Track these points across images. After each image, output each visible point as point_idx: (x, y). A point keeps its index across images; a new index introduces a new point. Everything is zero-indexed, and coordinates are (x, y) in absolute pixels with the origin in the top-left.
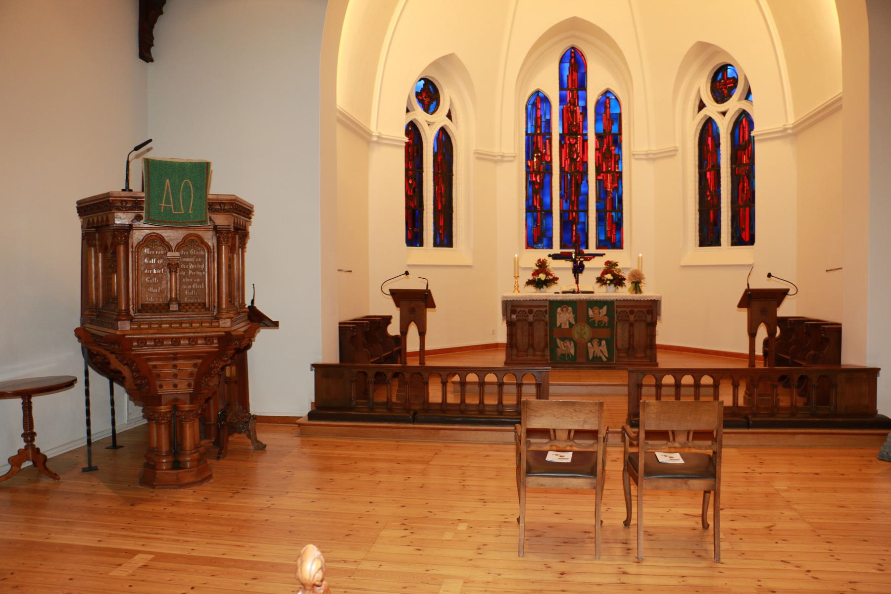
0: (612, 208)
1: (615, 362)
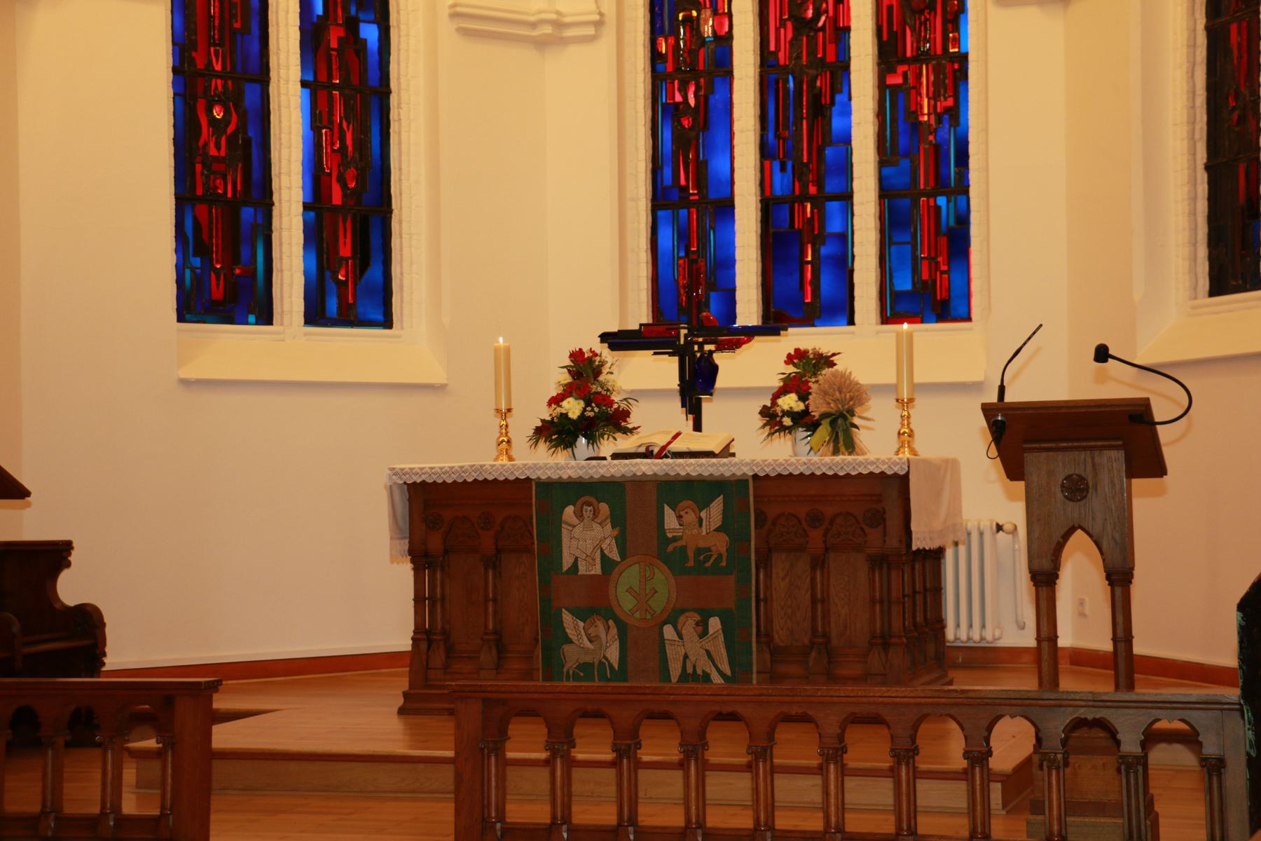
0: (936, 183)
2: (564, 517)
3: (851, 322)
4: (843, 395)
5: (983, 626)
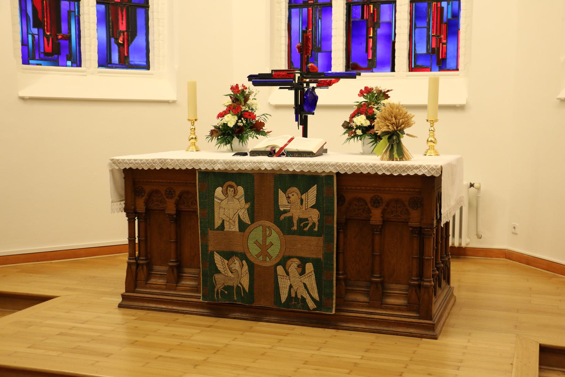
1: (334, 312)
2: (216, 194)
3: (393, 70)
4: (397, 121)
5: (460, 236)
